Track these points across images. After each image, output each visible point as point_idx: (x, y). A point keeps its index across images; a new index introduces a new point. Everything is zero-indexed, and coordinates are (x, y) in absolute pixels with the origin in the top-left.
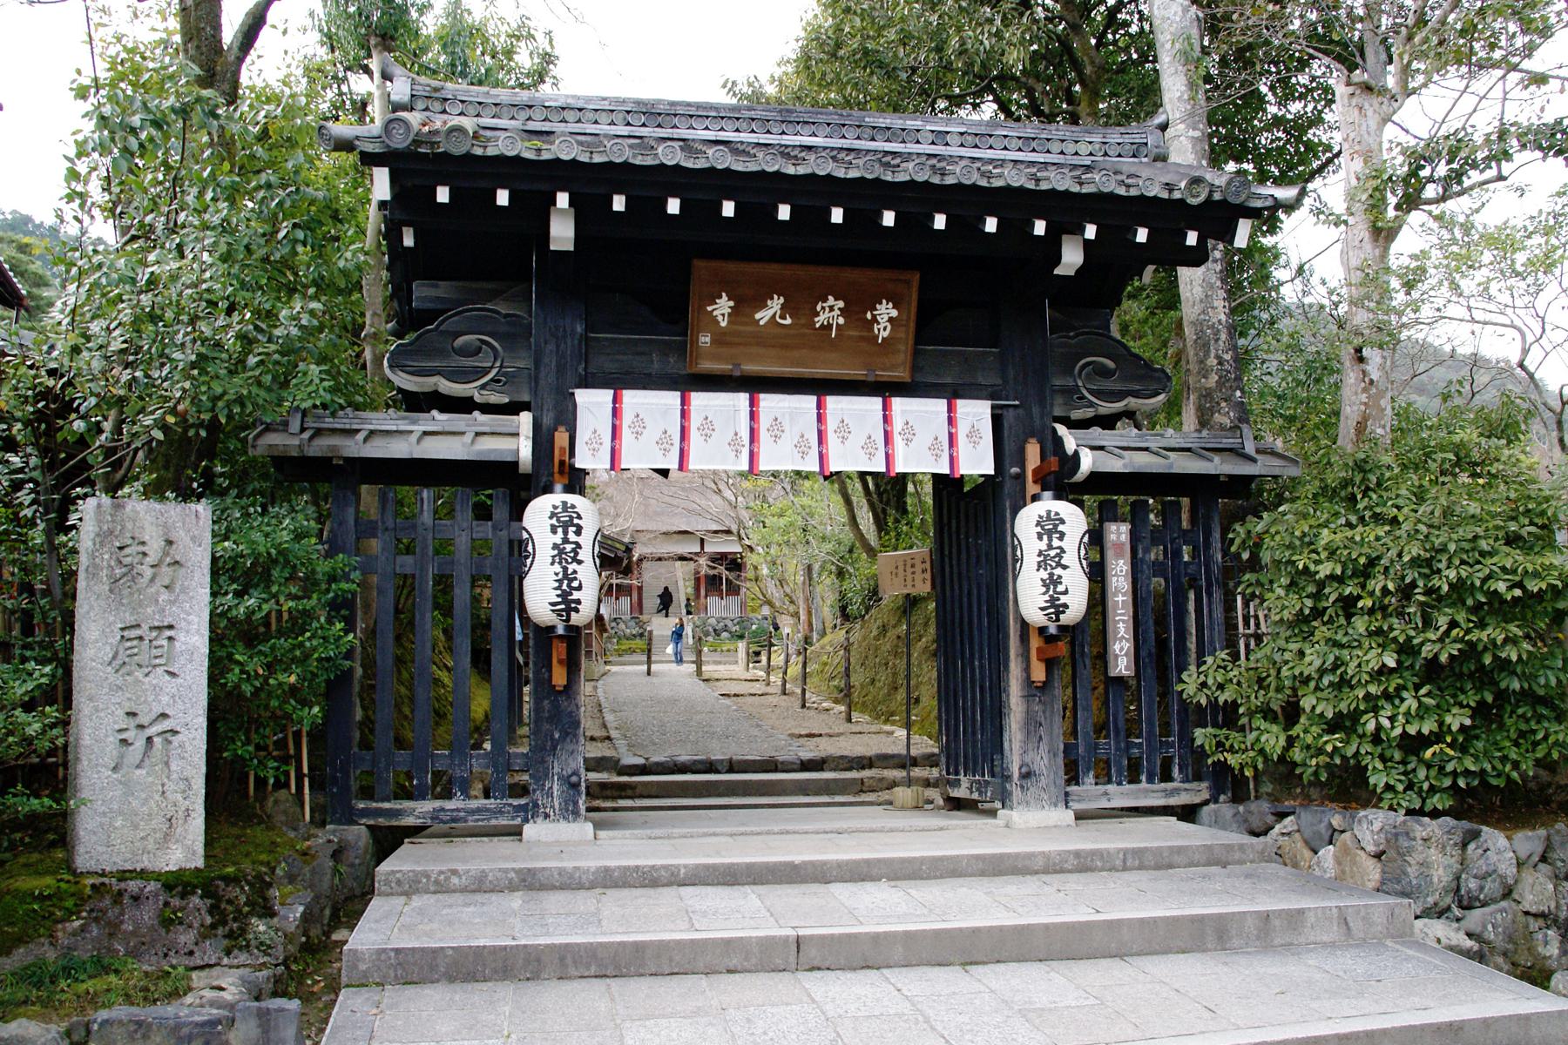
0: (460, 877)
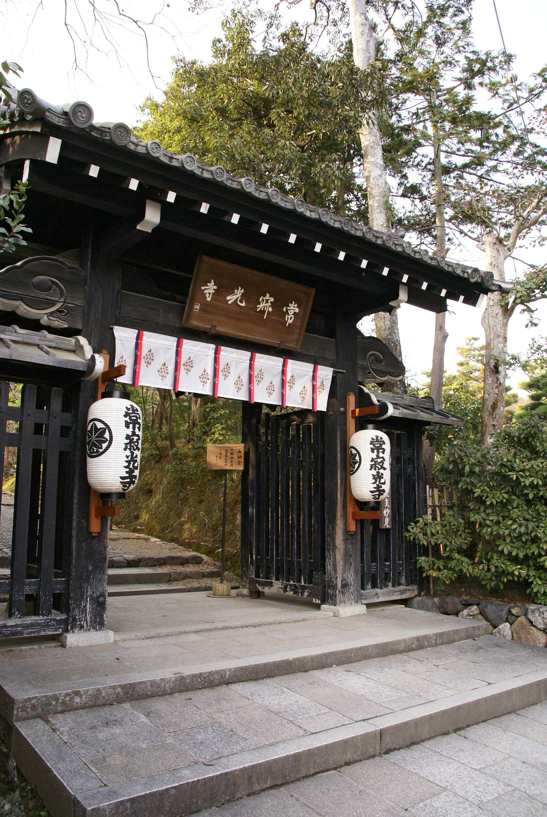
0: (81, 697)
